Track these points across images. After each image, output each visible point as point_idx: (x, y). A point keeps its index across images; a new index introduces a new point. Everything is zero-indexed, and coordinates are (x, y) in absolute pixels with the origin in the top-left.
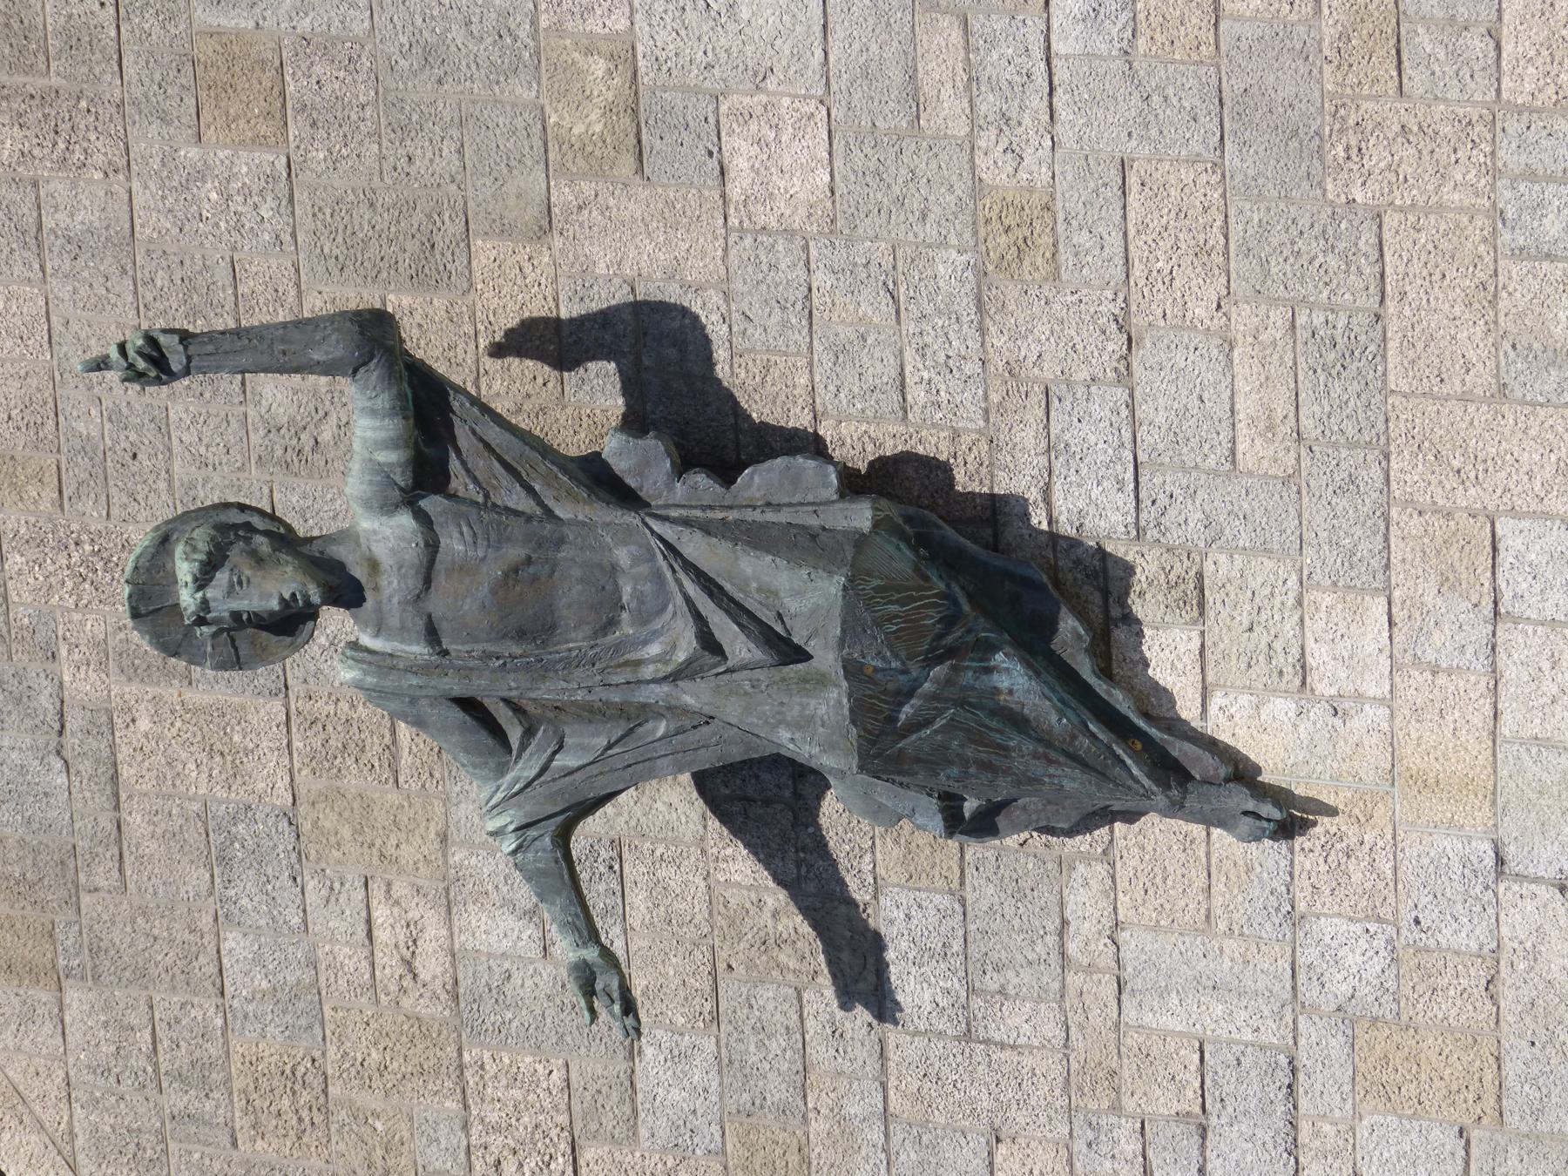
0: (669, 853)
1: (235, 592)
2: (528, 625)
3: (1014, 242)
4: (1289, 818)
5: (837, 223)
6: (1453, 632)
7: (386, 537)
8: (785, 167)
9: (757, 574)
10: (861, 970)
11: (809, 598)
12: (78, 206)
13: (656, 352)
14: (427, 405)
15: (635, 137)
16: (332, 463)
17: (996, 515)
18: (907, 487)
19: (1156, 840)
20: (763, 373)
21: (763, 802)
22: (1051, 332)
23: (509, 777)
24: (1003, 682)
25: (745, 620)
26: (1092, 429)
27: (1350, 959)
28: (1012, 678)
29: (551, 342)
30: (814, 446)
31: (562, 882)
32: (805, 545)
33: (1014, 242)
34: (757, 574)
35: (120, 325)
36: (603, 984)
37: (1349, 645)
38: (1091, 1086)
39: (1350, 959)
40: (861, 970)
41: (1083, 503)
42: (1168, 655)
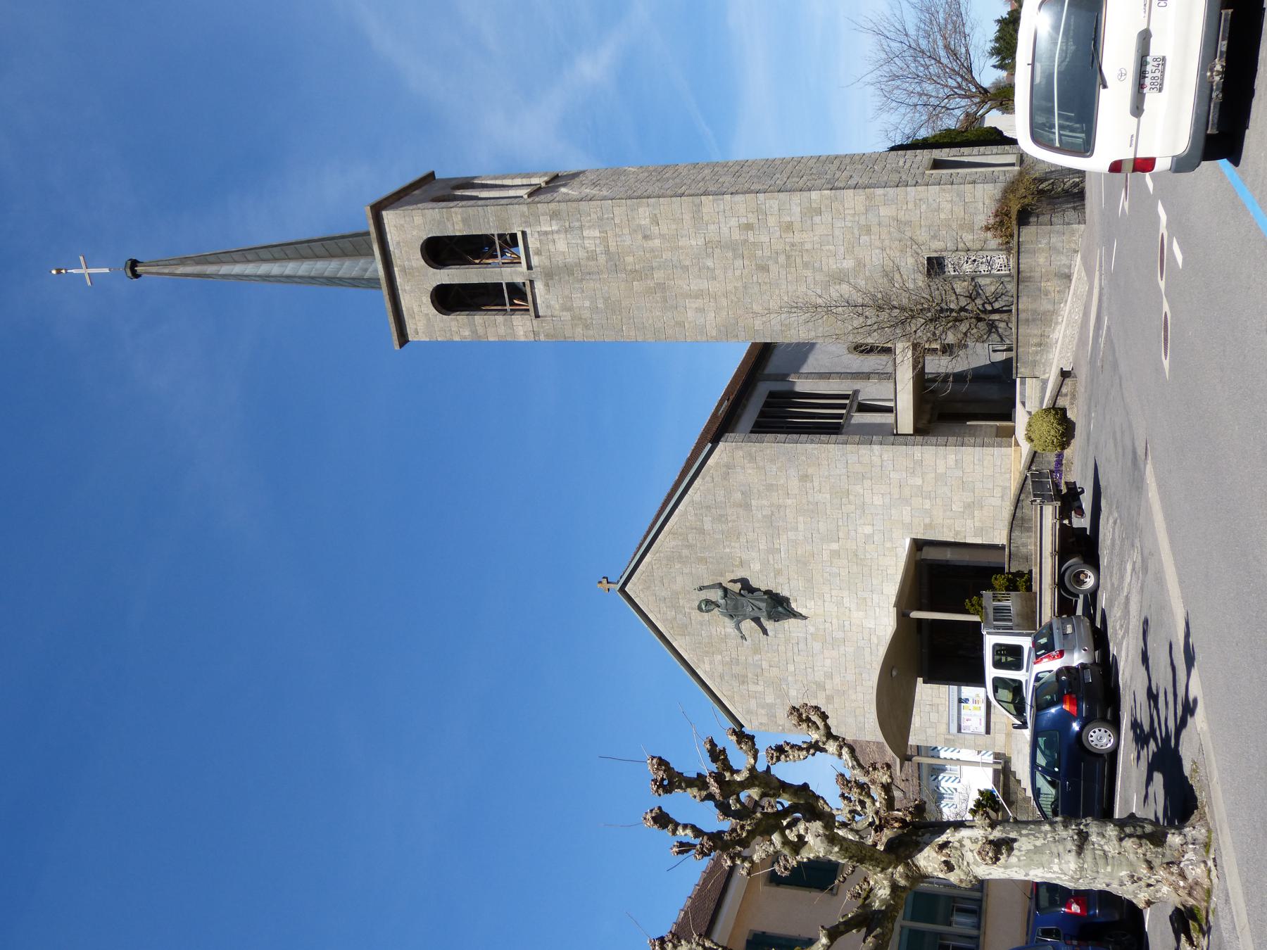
0: (748, 625)
1: (709, 605)
2: (736, 607)
3: (778, 573)
4: (805, 618)
5: (761, 571)
6: (820, 603)
7: (722, 602)
8: (756, 566)
9: (757, 603)
10: (765, 632)
11: (763, 605)
12: (686, 571)
13: (745, 583)
14: (725, 590)
15: (742, 564)
16: (716, 595)
17: (777, 594)
18: (768, 592)
19: (792, 621)
20: (754, 583)
21: (757, 620)
22: (781, 580)
23: (1021, 418)
24: (1076, 655)
25: (263, 254)
26: (786, 587)
27: (812, 629)
28: (780, 609)
29: (734, 581)
30: (759, 590)
31: (739, 629)
32: (761, 600)
33: (778, 573)
34: (757, 603)
35: (697, 586)
36: (743, 637)
37: (811, 604)
38: (787, 641)
39: (812, 629)
40: (765, 632)
41: (785, 593)
42: (793, 605)
